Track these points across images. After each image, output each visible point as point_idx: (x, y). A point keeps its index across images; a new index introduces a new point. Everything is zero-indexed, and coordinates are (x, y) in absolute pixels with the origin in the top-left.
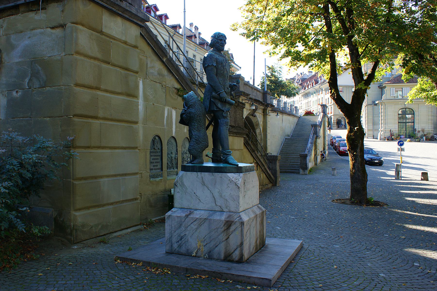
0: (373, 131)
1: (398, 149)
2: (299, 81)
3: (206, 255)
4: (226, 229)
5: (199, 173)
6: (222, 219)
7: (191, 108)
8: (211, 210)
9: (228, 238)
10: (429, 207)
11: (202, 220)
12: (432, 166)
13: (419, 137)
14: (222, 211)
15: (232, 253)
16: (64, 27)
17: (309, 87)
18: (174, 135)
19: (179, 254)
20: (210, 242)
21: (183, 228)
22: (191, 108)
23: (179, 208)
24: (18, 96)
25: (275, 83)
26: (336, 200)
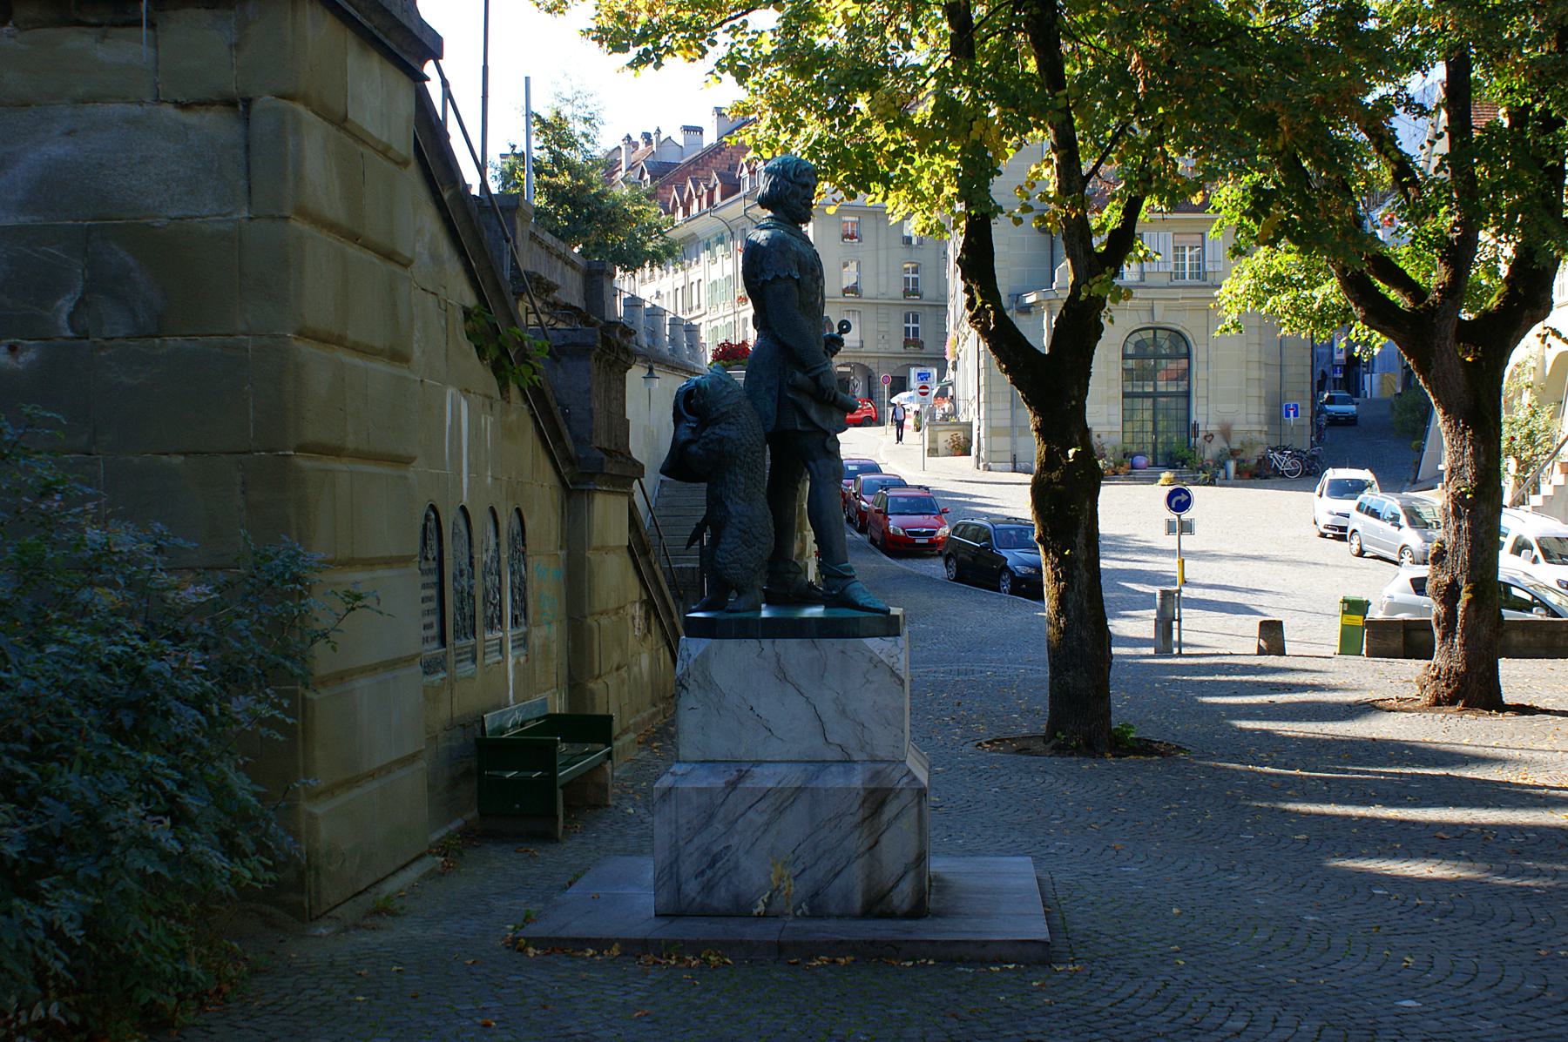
0: (1012, 436)
1: (1170, 524)
2: (641, 177)
3: (801, 907)
4: (869, 817)
5: (767, 643)
6: (852, 786)
7: (723, 425)
8: (808, 762)
9: (877, 842)
10: (1328, 749)
11: (786, 794)
12: (1278, 594)
13: (1211, 464)
14: (848, 761)
15: (890, 890)
16: (237, 106)
17: (694, 209)
18: (465, 500)
19: (705, 913)
20: (816, 863)
21: (718, 826)
22: (723, 425)
23: (696, 762)
24: (20, 367)
25: (572, 203)
26: (987, 743)
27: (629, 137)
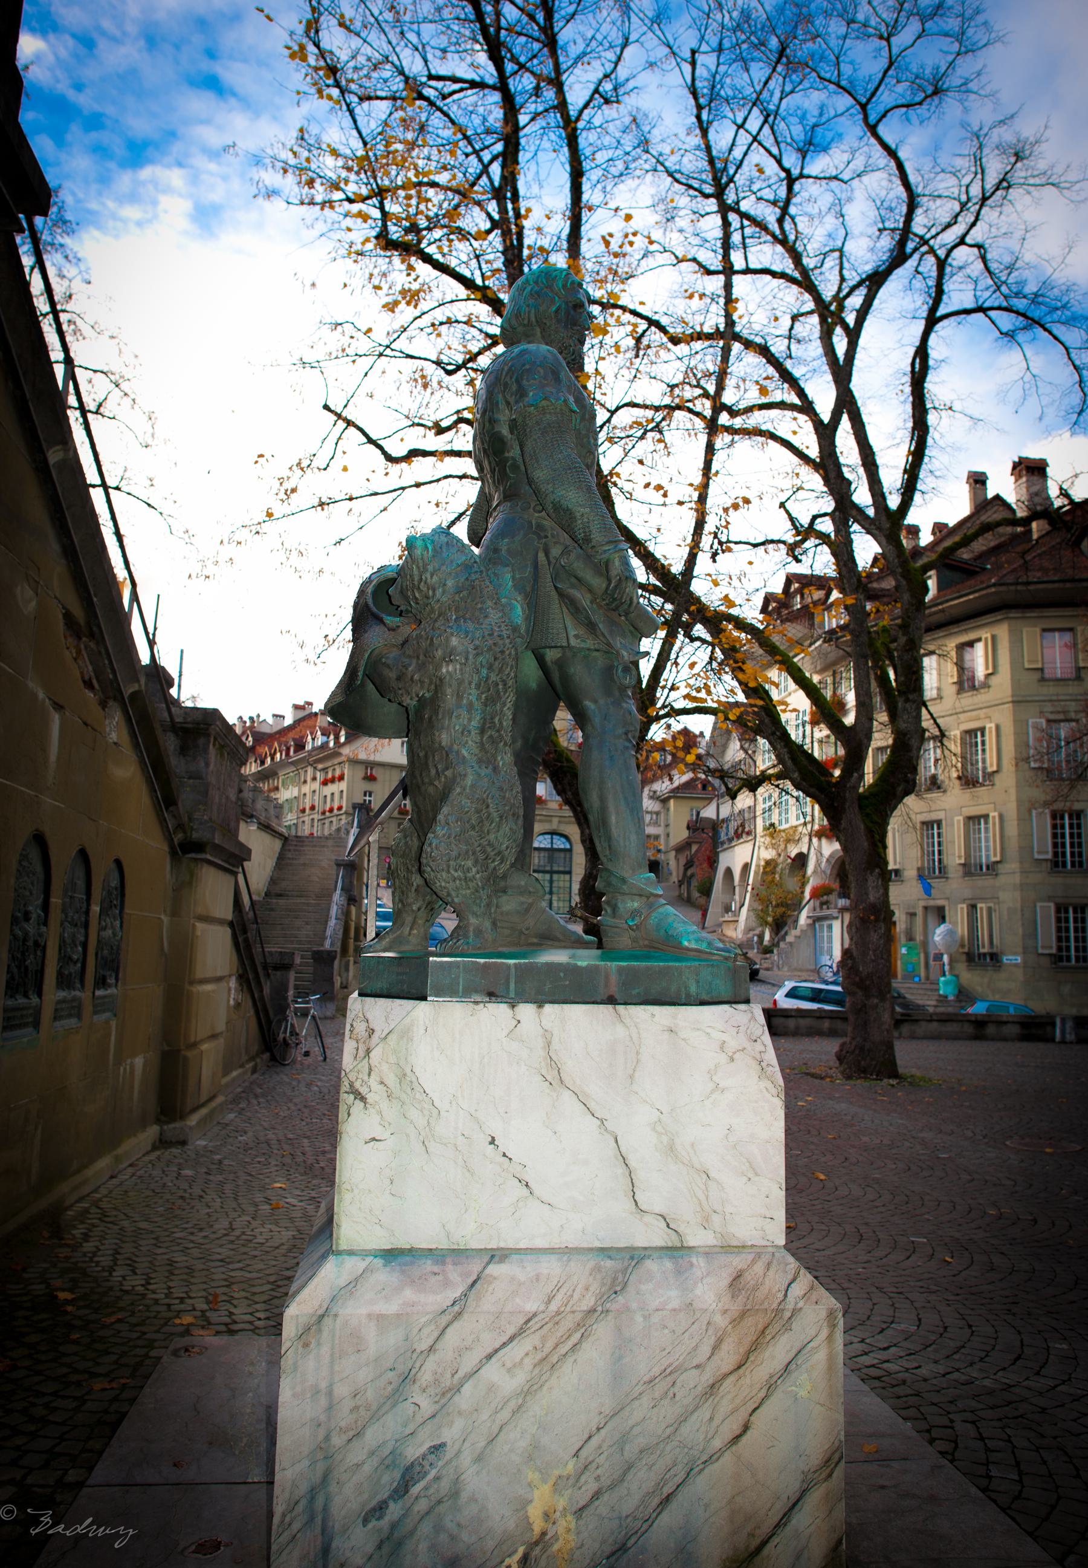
5: (526, 1010)
11: (568, 1323)
27: (241, 718)
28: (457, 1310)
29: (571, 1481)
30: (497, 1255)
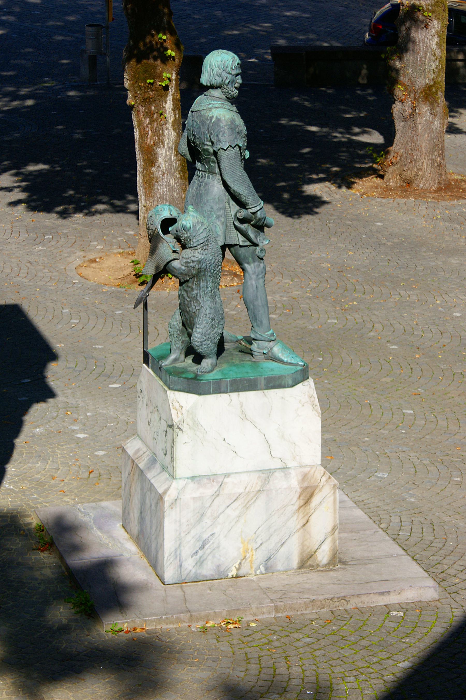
11: (252, 495)
28: (217, 495)
29: (254, 541)
30: (227, 475)
